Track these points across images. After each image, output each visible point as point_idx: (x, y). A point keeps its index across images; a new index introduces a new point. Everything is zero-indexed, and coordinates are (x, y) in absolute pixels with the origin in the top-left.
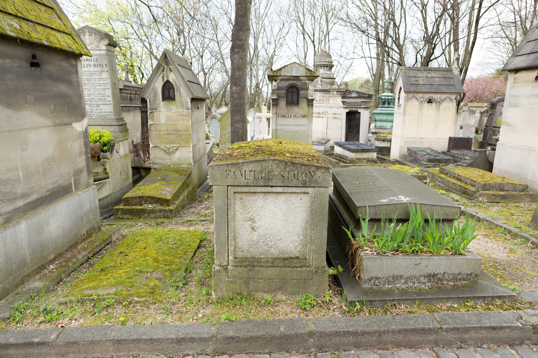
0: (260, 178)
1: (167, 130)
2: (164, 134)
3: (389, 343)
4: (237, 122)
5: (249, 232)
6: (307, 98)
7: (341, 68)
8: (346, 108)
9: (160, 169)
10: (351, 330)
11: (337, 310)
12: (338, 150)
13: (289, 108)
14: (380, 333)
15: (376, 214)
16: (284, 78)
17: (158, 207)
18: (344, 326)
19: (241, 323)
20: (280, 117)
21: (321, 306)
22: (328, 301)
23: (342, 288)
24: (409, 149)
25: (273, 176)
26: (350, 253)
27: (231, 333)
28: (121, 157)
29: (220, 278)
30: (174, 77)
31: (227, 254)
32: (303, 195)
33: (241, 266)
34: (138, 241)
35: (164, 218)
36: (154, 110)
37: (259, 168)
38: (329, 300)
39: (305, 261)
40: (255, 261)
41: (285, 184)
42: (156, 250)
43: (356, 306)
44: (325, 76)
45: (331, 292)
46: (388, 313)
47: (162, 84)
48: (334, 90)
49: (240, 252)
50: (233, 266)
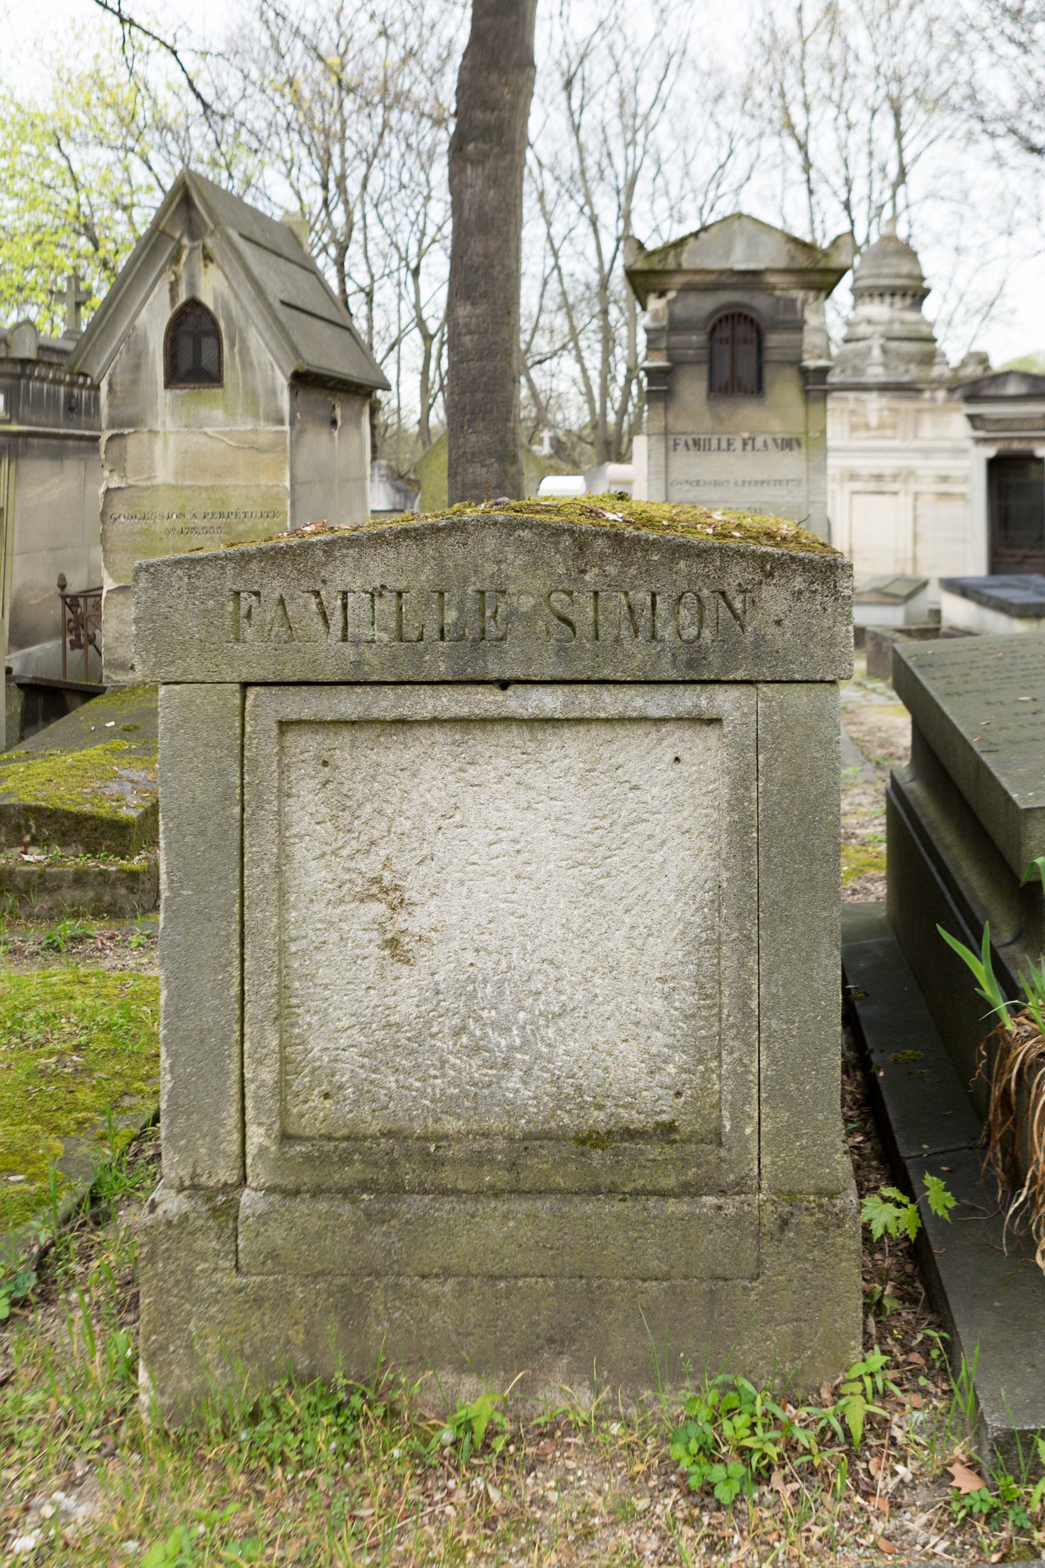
2: (168, 532)
6: (796, 363)
7: (962, 309)
8: (985, 441)
11: (922, 1496)
12: (958, 611)
13: (724, 409)
16: (698, 278)
17: (75, 860)
20: (681, 447)
25: (507, 620)
26: (996, 1092)
29: (188, 1272)
30: (223, 285)
31: (234, 1110)
33: (317, 1192)
35: (97, 915)
38: (870, 1417)
40: (408, 1156)
41: (581, 669)
44: (897, 329)
45: (876, 1359)
47: (168, 314)
48: (937, 383)
49: (316, 1100)
50: (270, 1190)
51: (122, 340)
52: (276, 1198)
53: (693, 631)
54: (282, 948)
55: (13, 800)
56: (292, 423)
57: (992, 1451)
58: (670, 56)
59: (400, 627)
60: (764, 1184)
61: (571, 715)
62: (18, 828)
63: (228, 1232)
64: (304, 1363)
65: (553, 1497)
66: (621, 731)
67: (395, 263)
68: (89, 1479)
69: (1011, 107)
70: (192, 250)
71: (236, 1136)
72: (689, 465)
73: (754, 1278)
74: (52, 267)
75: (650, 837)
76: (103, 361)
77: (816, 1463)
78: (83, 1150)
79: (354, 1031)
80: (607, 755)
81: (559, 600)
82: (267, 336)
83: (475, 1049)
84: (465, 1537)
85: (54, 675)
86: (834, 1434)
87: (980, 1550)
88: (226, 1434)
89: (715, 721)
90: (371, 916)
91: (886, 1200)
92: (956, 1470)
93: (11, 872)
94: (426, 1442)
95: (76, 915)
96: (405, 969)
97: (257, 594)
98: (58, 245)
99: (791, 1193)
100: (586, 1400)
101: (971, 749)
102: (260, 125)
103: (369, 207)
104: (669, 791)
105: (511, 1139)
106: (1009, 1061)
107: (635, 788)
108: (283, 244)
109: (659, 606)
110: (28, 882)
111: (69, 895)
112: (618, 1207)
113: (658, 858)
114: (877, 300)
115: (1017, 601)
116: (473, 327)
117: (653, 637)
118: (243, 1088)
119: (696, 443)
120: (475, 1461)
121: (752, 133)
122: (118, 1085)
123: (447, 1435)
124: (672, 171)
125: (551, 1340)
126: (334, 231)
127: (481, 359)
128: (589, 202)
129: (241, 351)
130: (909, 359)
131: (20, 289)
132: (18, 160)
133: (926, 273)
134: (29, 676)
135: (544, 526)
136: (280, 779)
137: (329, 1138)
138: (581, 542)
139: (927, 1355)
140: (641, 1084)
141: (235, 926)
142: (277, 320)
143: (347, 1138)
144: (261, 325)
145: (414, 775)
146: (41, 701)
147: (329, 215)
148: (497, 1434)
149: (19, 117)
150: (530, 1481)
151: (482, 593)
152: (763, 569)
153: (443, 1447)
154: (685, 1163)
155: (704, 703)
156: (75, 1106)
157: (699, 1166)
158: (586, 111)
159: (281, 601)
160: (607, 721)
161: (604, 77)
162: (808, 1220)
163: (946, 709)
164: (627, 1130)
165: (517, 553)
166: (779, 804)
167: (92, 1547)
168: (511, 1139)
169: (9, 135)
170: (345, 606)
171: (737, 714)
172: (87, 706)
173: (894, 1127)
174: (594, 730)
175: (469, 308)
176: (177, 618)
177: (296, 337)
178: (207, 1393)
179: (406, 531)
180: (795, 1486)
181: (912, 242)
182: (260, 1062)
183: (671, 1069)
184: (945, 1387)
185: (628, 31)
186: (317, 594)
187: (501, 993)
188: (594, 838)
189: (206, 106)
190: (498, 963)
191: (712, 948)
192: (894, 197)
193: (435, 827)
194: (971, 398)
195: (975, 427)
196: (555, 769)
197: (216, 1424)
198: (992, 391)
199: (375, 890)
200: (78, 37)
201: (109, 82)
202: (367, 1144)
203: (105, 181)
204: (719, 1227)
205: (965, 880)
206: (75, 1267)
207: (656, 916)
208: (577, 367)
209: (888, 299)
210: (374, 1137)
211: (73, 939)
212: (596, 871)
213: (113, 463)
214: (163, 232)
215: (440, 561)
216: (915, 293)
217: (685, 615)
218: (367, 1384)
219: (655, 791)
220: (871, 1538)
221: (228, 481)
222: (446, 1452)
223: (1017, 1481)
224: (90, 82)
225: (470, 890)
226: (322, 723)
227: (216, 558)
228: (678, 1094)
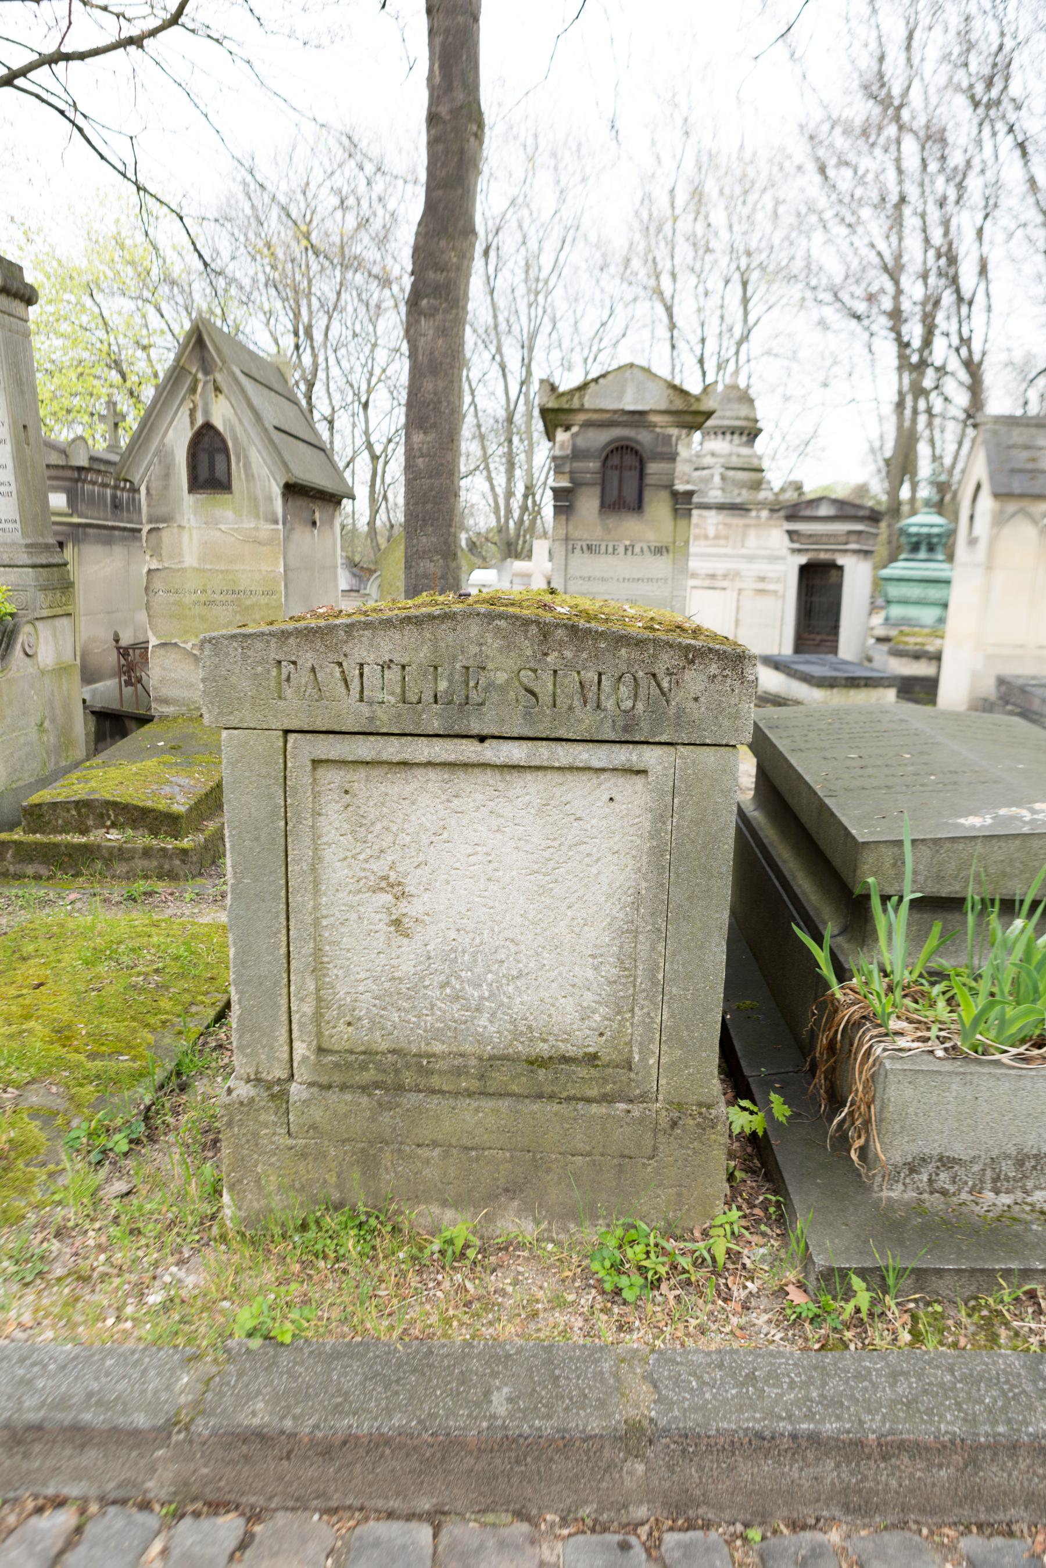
0: (427, 697)
1: (204, 591)
2: (195, 603)
3: (1014, 1503)
4: (423, 554)
5: (379, 941)
6: (669, 487)
7: (784, 446)
8: (799, 551)
9: (175, 719)
10: (830, 1427)
11: (764, 1303)
13: (611, 521)
14: (973, 1454)
15: (939, 878)
17: (142, 839)
18: (796, 1402)
19: (318, 1354)
20: (578, 551)
21: (688, 1283)
22: (721, 1257)
23: (786, 1194)
24: (1001, 681)
25: (486, 690)
27: (259, 1414)
28: (43, 673)
29: (256, 1135)
30: (229, 412)
31: (284, 1031)
32: (621, 780)
33: (343, 1087)
34: (24, 959)
35: (160, 877)
36: (164, 521)
37: (425, 653)
38: (728, 1251)
39: (623, 1074)
40: (408, 1067)
42: (77, 992)
43: (849, 1294)
44: (735, 461)
46: (1003, 1332)
48: (762, 505)
49: (341, 1026)
50: (311, 1085)
51: (155, 455)
52: (315, 1090)
53: (629, 704)
54: (316, 922)
55: (97, 796)
56: (284, 524)
57: (818, 1279)
58: (567, 229)
59: (404, 692)
60: (660, 1097)
61: (533, 764)
62: (101, 816)
63: (282, 1110)
64: (336, 1196)
65: (510, 1289)
66: (569, 776)
67: (350, 398)
68: (193, 1260)
69: (838, 280)
70: (206, 383)
71: (286, 1048)
72: (583, 564)
73: (650, 1158)
74: (91, 395)
75: (589, 855)
76: (142, 471)
77: (693, 1279)
78: (167, 1040)
79: (369, 981)
80: (558, 794)
81: (526, 676)
82: (265, 455)
83: (456, 998)
84: (451, 1312)
85: (115, 706)
86: (704, 1260)
87: (806, 1340)
88: (284, 1236)
89: (642, 772)
90: (380, 904)
91: (744, 1109)
92: (790, 1289)
93: (99, 846)
94: (421, 1249)
95: (146, 877)
96: (406, 941)
97: (294, 663)
98: (95, 377)
99: (679, 1104)
100: (530, 1228)
101: (816, 794)
102: (246, 282)
103: (330, 352)
104: (604, 823)
105: (480, 1059)
106: (837, 1019)
107: (579, 819)
108: (270, 379)
109: (604, 682)
110: (111, 854)
111: (140, 864)
112: (556, 1107)
113: (594, 870)
114: (720, 437)
115: (816, 674)
116: (425, 451)
117: (598, 707)
118: (290, 1016)
119: (589, 547)
120: (456, 1264)
121: (629, 297)
122: (187, 997)
123: (436, 1247)
124: (565, 327)
125: (507, 1190)
126: (304, 371)
127: (430, 477)
128: (499, 350)
129: (245, 465)
130: (742, 485)
131: (69, 411)
132: (61, 306)
133: (759, 417)
134: (98, 706)
135: (516, 617)
136: (313, 802)
137: (351, 1052)
138: (545, 631)
139: (766, 1210)
140: (575, 1027)
141: (283, 906)
142: (271, 441)
143: (364, 1053)
144: (260, 445)
145: (413, 803)
146: (108, 724)
147: (299, 357)
148: (469, 1247)
149: (60, 271)
150: (493, 1278)
151: (467, 668)
152: (686, 657)
153: (433, 1253)
154: (605, 1080)
155: (634, 758)
156: (158, 1011)
157: (614, 1083)
158: (499, 275)
159: (313, 669)
160: (559, 768)
161: (513, 250)
162: (691, 1122)
163: (793, 761)
164: (564, 1057)
165: (495, 638)
166: (687, 835)
167: (199, 1303)
168: (480, 1059)
169: (54, 286)
170: (361, 675)
171: (659, 768)
172: (142, 730)
173: (739, 1054)
174: (550, 775)
175: (422, 436)
176: (234, 680)
177: (287, 456)
178: (271, 1211)
179: (409, 618)
180: (677, 1292)
181: (750, 391)
182: (302, 1000)
183: (597, 1017)
184: (778, 1232)
185: (534, 206)
186: (340, 664)
187: (475, 961)
188: (546, 854)
189: (206, 264)
190: (473, 939)
191: (631, 936)
192: (737, 353)
193: (428, 842)
194: (790, 518)
195: (792, 541)
196: (518, 803)
197: (277, 1231)
198: (808, 513)
199: (383, 884)
200: (102, 204)
201: (128, 242)
202: (378, 1057)
203: (129, 325)
204: (628, 1124)
205: (800, 886)
206: (169, 1119)
207: (590, 911)
208: (487, 485)
209: (728, 437)
210: (383, 1053)
211: (145, 894)
212: (547, 878)
213: (153, 549)
214: (183, 368)
215: (435, 641)
216: (751, 433)
217: (624, 691)
218: (380, 1211)
219: (593, 822)
220: (728, 1329)
221: (238, 567)
222: (435, 1257)
223: (834, 1298)
224: (113, 242)
225: (454, 888)
226: (344, 762)
227: (263, 634)
228: (601, 1034)
